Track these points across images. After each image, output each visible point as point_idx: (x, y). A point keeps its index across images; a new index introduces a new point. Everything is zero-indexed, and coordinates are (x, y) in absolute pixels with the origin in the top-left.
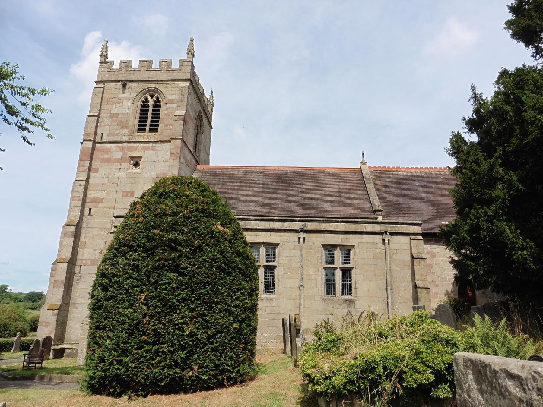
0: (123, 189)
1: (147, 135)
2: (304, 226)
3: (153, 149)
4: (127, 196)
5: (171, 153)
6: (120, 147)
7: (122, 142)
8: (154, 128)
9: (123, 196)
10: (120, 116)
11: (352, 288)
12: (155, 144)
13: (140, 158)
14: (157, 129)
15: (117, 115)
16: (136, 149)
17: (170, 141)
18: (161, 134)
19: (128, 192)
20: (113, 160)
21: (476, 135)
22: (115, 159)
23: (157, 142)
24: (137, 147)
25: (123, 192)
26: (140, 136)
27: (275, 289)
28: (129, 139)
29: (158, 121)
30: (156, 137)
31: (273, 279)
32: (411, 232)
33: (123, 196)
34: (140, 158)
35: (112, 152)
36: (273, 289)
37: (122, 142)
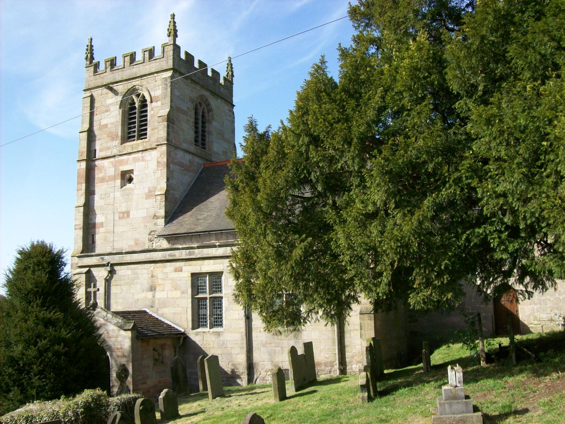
0: (119, 210)
1: (138, 144)
2: (190, 254)
3: (143, 160)
4: (123, 217)
5: (158, 162)
6: (112, 163)
7: (114, 156)
8: (142, 134)
9: (120, 219)
10: (109, 126)
11: (224, 318)
12: (145, 153)
13: (131, 171)
14: (146, 134)
15: (106, 125)
16: (127, 162)
17: (156, 148)
18: (150, 140)
19: (123, 213)
20: (107, 178)
21: (238, 156)
22: (109, 177)
23: (146, 150)
24: (128, 159)
25: (120, 213)
26: (130, 146)
27: (224, 322)
28: (120, 151)
29: (146, 125)
30: (145, 144)
31: (221, 311)
32: (157, 259)
33: (120, 219)
34: (131, 171)
35: (105, 170)
36: (221, 322)
37: (114, 156)
